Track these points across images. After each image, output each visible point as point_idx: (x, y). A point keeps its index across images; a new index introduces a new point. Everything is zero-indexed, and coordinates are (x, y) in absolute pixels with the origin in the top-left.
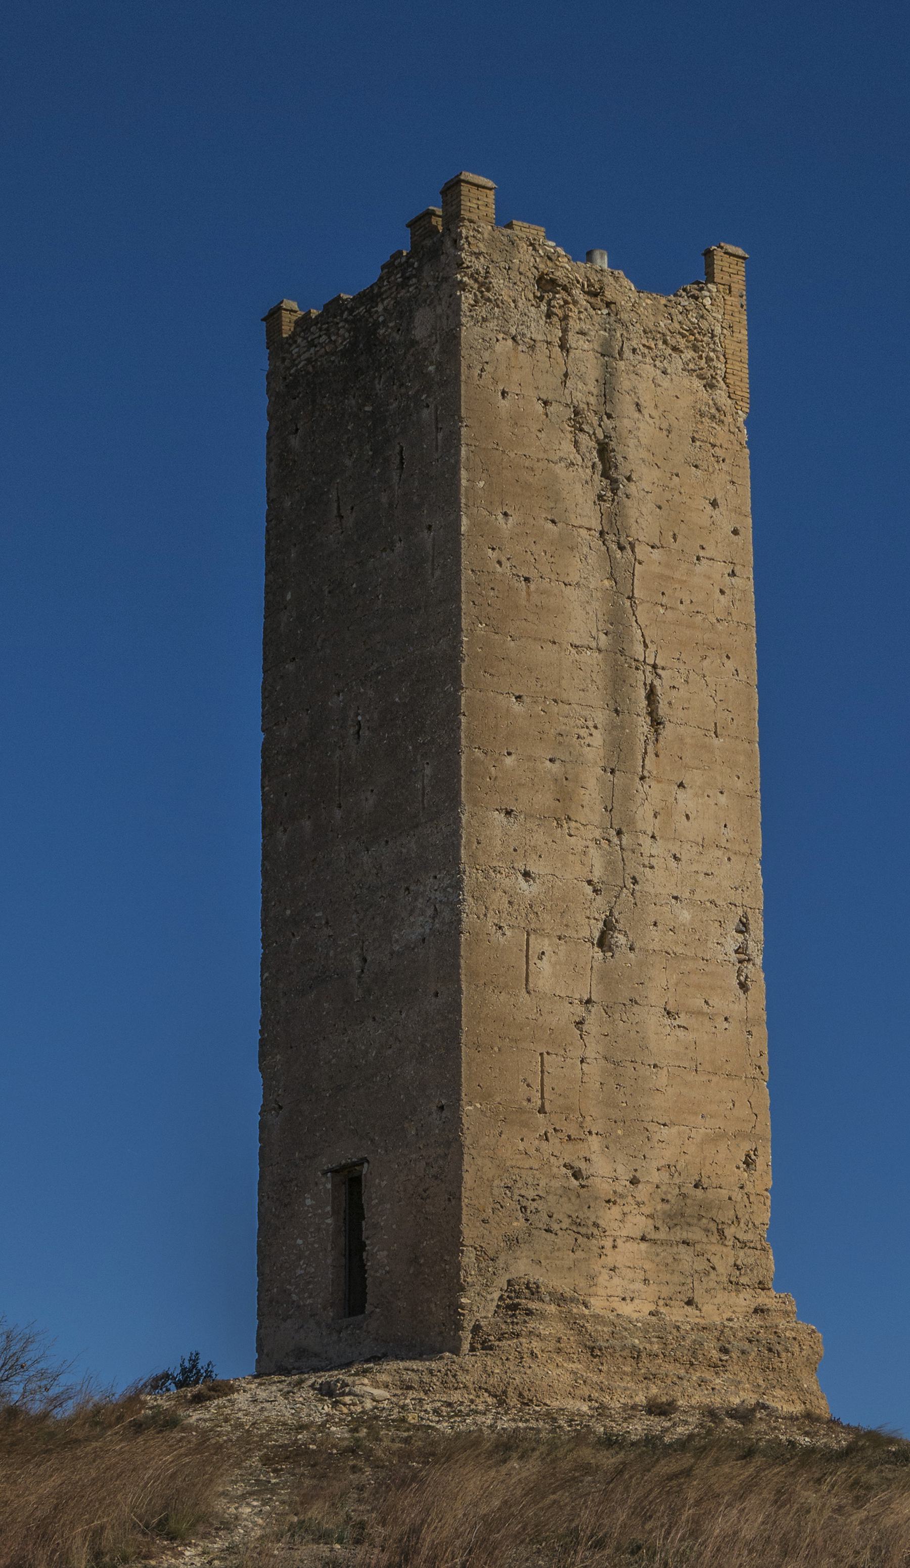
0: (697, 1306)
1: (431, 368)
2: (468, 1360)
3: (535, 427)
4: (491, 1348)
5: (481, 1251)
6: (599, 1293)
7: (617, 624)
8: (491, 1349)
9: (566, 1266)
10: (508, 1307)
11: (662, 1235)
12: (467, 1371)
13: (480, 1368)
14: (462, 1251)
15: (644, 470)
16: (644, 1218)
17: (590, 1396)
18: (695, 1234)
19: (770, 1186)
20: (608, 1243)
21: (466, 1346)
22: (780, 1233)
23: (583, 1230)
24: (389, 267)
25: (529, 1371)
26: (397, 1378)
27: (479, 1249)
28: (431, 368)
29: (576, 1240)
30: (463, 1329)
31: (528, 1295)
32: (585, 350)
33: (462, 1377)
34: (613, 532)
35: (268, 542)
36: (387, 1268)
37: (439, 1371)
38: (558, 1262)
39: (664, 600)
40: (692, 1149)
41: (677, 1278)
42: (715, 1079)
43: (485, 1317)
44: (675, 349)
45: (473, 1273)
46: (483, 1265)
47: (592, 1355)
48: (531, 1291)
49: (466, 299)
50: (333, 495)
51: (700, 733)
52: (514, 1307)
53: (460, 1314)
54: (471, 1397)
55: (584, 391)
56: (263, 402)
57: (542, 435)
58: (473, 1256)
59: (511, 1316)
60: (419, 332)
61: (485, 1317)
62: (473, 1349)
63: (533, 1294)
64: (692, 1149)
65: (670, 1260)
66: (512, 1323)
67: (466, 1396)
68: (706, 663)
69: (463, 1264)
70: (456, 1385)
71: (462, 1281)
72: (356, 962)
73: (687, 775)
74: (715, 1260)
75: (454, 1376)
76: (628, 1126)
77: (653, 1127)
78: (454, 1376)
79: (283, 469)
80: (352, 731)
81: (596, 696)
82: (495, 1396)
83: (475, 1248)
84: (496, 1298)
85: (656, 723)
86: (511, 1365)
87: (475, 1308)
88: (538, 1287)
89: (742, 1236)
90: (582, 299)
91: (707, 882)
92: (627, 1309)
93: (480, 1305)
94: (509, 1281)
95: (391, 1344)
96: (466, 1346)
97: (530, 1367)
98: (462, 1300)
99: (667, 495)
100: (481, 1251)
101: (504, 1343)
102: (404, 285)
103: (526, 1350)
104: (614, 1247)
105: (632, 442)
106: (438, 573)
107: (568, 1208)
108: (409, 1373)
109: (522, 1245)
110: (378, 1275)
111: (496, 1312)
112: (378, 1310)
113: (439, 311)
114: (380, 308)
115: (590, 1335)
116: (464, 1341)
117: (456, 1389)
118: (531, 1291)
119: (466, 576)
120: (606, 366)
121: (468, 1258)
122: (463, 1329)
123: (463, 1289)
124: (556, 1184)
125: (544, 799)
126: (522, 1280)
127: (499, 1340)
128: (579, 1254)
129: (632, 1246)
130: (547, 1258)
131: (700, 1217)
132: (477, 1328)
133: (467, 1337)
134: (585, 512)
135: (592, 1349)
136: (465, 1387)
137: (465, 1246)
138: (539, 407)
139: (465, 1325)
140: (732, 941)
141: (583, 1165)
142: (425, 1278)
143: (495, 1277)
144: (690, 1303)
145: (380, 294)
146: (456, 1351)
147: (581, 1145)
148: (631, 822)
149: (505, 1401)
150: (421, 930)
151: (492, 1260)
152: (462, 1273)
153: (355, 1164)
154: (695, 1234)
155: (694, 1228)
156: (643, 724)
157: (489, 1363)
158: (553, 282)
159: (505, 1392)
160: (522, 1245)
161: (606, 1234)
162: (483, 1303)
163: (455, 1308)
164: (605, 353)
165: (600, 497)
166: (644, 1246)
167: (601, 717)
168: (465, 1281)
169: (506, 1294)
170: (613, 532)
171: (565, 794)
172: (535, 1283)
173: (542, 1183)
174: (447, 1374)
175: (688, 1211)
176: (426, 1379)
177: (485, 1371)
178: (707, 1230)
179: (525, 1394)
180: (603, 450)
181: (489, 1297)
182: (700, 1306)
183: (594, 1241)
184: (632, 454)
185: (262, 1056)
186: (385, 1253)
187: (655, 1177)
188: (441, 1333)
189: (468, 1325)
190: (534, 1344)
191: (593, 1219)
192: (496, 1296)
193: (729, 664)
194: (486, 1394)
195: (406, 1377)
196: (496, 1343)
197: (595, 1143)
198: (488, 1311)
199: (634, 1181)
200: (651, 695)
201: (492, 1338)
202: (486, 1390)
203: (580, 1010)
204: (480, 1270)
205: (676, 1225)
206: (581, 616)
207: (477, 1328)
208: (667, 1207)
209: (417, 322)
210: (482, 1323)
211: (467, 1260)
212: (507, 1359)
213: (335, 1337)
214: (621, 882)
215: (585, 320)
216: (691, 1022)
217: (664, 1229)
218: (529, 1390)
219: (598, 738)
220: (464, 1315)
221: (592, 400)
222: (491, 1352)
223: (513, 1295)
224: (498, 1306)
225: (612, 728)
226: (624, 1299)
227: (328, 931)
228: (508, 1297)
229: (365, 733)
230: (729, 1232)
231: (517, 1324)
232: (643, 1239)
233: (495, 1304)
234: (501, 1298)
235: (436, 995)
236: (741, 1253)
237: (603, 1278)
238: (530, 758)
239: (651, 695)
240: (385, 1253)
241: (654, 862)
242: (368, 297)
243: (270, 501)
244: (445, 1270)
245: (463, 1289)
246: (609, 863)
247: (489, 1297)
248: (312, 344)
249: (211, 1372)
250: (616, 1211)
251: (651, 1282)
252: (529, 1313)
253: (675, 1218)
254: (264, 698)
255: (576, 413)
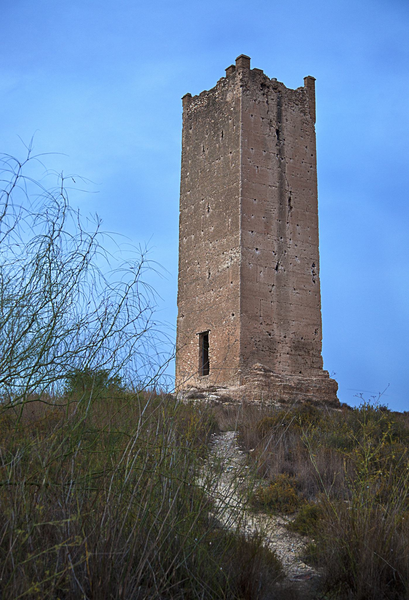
1: (232, 109)
3: (260, 125)
11: (293, 353)
15: (288, 138)
18: (302, 353)
20: (279, 355)
23: (272, 351)
24: (219, 82)
28: (232, 109)
32: (273, 103)
35: (182, 159)
39: (293, 173)
40: (301, 328)
41: (297, 365)
42: (307, 308)
44: (296, 105)
50: (202, 145)
51: (303, 210)
56: (182, 121)
57: (262, 127)
60: (228, 99)
64: (301, 328)
68: (304, 191)
72: (207, 274)
74: (307, 360)
76: (284, 322)
77: (290, 322)
79: (187, 138)
80: (207, 210)
81: (276, 199)
89: (314, 353)
90: (271, 90)
91: (304, 252)
99: (294, 145)
102: (224, 86)
105: (285, 130)
106: (233, 165)
107: (268, 344)
113: (235, 93)
114: (217, 93)
120: (279, 109)
124: (265, 337)
125: (262, 228)
128: (271, 358)
129: (285, 356)
131: (303, 348)
134: (273, 149)
138: (261, 119)
141: (272, 332)
144: (300, 373)
145: (217, 89)
147: (271, 326)
148: (285, 235)
150: (227, 265)
153: (206, 332)
154: (302, 353)
158: (265, 85)
165: (277, 145)
166: (288, 355)
167: (277, 205)
171: (267, 226)
173: (261, 337)
175: (300, 346)
178: (305, 352)
185: (178, 302)
187: (292, 336)
193: (311, 192)
199: (285, 337)
203: (270, 287)
208: (294, 345)
209: (228, 96)
213: (199, 382)
216: (301, 292)
217: (293, 351)
221: (275, 118)
225: (280, 209)
227: (198, 266)
229: (211, 210)
230: (311, 352)
232: (288, 354)
235: (232, 283)
236: (314, 358)
237: (277, 365)
238: (258, 217)
241: (290, 246)
242: (213, 91)
243: (183, 148)
246: (279, 246)
248: (196, 104)
250: (280, 345)
253: (296, 348)
254: (180, 202)
255: (271, 121)
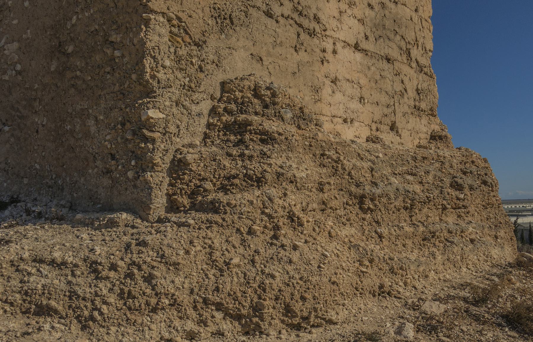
0: (397, 132)
2: (172, 239)
4: (214, 208)
5: (179, 27)
6: (324, 112)
8: (216, 211)
9: (290, 70)
10: (227, 128)
12: (176, 264)
13: (202, 257)
14: (147, 22)
16: (356, 21)
17: (381, 287)
19: (431, 14)
21: (159, 202)
22: (437, 56)
25: (295, 256)
26: (15, 283)
27: (175, 22)
29: (299, 35)
30: (153, 167)
31: (259, 108)
33: (165, 280)
36: (19, 67)
37: (113, 267)
38: (281, 63)
43: (191, 145)
45: (167, 63)
46: (183, 52)
47: (360, 208)
48: (263, 101)
52: (241, 128)
53: (146, 139)
54: (190, 325)
58: (164, 31)
59: (236, 145)
61: (191, 145)
62: (173, 206)
63: (266, 106)
65: (378, 77)
66: (242, 155)
67: (177, 323)
69: (149, 44)
70: (153, 301)
71: (148, 77)
75: (149, 279)
78: (149, 279)
82: (238, 317)
83: (169, 20)
84: (206, 112)
86: (257, 243)
87: (172, 129)
88: (274, 95)
92: (348, 133)
93: (179, 123)
94: (223, 84)
95: (26, 181)
96: (159, 202)
97: (295, 248)
98: (151, 113)
100: (179, 27)
101: (237, 198)
103: (281, 212)
104: (335, 52)
108: (45, 269)
109: (238, 29)
110: (6, 78)
111: (206, 136)
112: (6, 128)
115: (349, 174)
116: (156, 191)
117: (154, 310)
118: (263, 101)
121: (157, 35)
122: (153, 167)
123: (149, 93)
126: (246, 83)
127: (224, 189)
130: (269, 54)
132: (178, 166)
133: (159, 180)
135: (361, 199)
136: (175, 304)
137: (152, 11)
139: (158, 160)
142: (77, 77)
143: (201, 75)
146: (140, 209)
149: (258, 325)
151: (197, 44)
152: (148, 62)
155: (391, 44)
157: (217, 244)
159: (257, 309)
160: (238, 29)
161: (328, 33)
162: (185, 119)
163: (141, 129)
166: (359, 56)
168: (153, 77)
169: (223, 106)
172: (268, 88)
174: (130, 275)
176: (84, 285)
177: (213, 263)
179: (297, 306)
181: (195, 109)
182: (400, 131)
183: (316, 41)
186: (16, 45)
188: (108, 172)
189: (162, 160)
190: (292, 198)
191: (314, 10)
192: (206, 106)
194: (219, 315)
195: (36, 282)
196: (223, 198)
198: (193, 134)
201: (208, 185)
202: (219, 307)
204: (178, 60)
205: (267, 68)
207: (178, 166)
210: (189, 157)
211: (156, 38)
212: (251, 232)
218: (303, 299)
220: (153, 141)
222: (217, 218)
223: (233, 106)
224: (209, 126)
226: (345, 121)
228: (225, 110)
231: (251, 158)
233: (204, 121)
234: (213, 111)
240: (16, 45)
244: (113, 59)
245: (149, 93)
247: (195, 109)
251: (366, 101)
252: (267, 138)
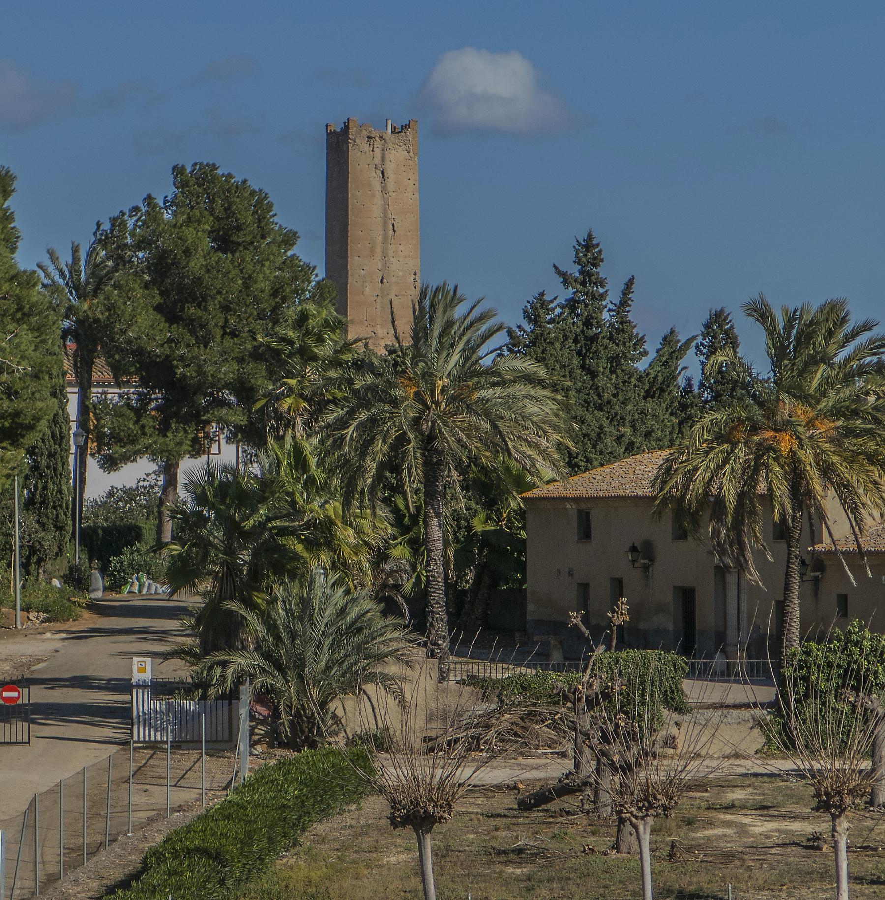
7: (385, 211)
32: (378, 151)
34: (384, 189)
49: (350, 145)
55: (377, 160)
73: (400, 548)
85: (395, 231)
119: (350, 206)
140: (413, 277)
156: (391, 232)
164: (383, 150)
167: (381, 232)
170: (384, 189)
180: (383, 173)
184: (389, 173)
197: (378, 326)
200: (393, 225)
206: (376, 211)
214: (386, 267)
215: (378, 143)
219: (380, 237)
239: (393, 225)
249: (440, 822)
